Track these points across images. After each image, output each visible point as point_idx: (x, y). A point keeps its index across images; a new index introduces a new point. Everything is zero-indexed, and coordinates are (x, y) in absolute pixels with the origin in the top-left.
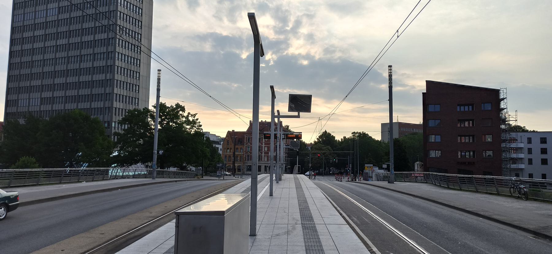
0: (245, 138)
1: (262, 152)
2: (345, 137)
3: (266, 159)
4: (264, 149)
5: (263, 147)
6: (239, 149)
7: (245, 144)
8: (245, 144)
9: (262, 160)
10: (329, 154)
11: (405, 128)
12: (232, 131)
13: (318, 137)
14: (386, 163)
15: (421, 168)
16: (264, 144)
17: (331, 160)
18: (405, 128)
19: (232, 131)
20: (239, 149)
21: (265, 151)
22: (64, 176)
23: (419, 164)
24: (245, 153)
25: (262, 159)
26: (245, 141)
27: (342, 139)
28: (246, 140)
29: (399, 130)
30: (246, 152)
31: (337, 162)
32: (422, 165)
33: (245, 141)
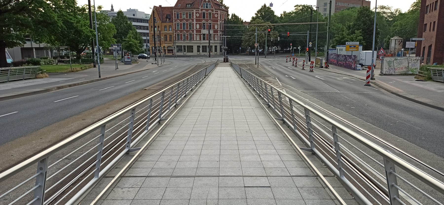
0: (174, 14)
1: (194, 30)
2: (285, 12)
3: (198, 39)
4: (196, 27)
5: (195, 25)
6: (168, 27)
7: (174, 21)
8: (174, 21)
9: (193, 39)
10: (133, 37)
11: (341, 3)
12: (159, 6)
13: (256, 13)
14: (414, 39)
15: (399, 45)
16: (195, 20)
17: (272, 38)
18: (341, 3)
19: (159, 6)
20: (168, 27)
21: (196, 28)
22: (10, 75)
23: (398, 39)
24: (174, 31)
25: (193, 38)
26: (174, 17)
27: (281, 15)
28: (175, 16)
29: (336, 6)
30: (175, 31)
31: (279, 40)
32: (402, 41)
33: (174, 17)
